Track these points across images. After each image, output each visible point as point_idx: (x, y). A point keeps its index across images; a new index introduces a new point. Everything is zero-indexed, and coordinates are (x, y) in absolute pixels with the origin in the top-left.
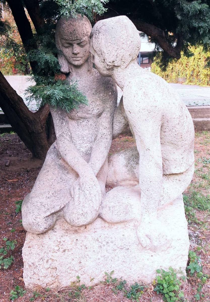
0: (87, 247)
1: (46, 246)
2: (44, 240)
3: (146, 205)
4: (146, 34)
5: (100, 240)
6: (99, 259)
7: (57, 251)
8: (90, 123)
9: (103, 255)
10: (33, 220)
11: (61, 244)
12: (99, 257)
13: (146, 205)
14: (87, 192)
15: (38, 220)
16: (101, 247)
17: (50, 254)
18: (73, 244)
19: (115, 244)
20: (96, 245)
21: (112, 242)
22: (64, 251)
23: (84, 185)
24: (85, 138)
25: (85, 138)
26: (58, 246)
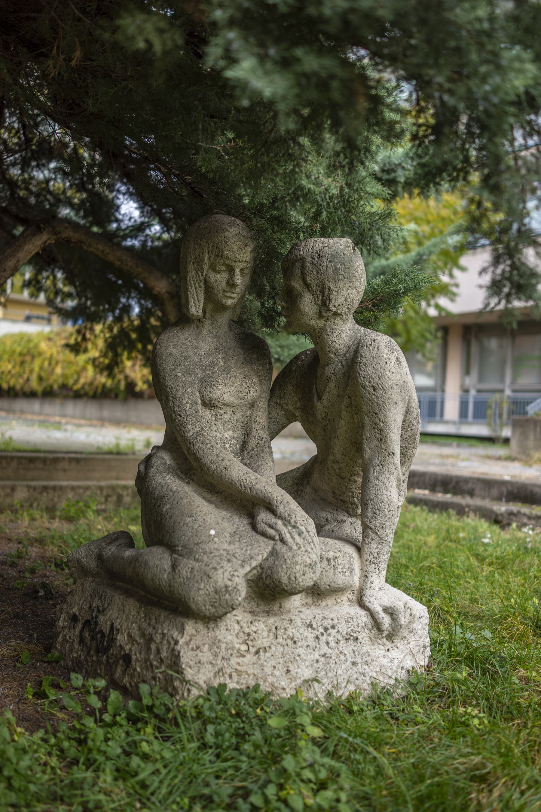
0: (295, 639)
1: (223, 646)
2: (218, 632)
3: (376, 555)
4: (101, 234)
5: (315, 626)
6: (317, 661)
7: (245, 654)
8: (235, 417)
9: (322, 652)
10: (226, 580)
11: (252, 637)
12: (317, 656)
13: (376, 555)
14: (303, 528)
15: (237, 580)
16: (317, 638)
17: (234, 661)
18: (272, 636)
19: (338, 631)
20: (310, 635)
21: (333, 627)
22: (257, 652)
23: (293, 517)
24: (227, 446)
25: (227, 446)
26: (245, 642)
